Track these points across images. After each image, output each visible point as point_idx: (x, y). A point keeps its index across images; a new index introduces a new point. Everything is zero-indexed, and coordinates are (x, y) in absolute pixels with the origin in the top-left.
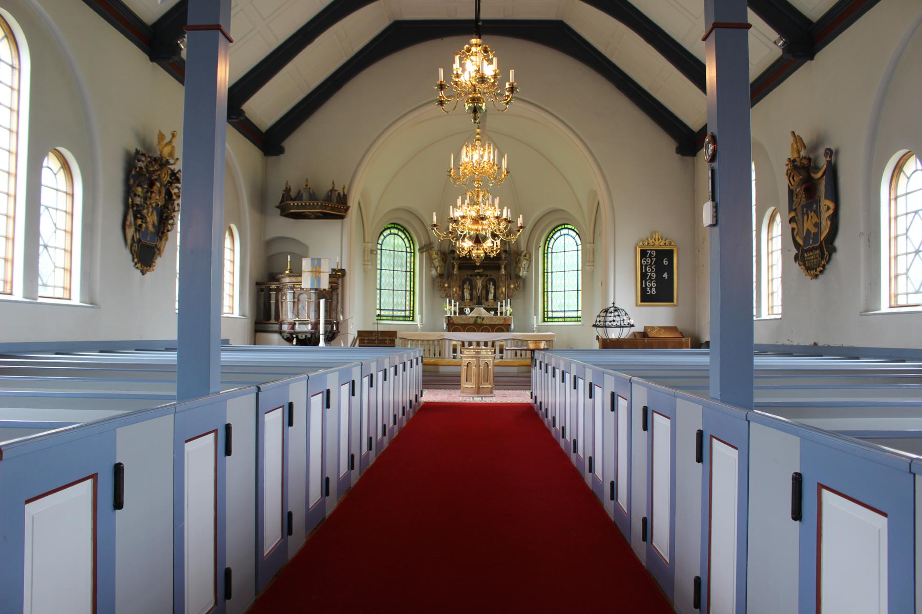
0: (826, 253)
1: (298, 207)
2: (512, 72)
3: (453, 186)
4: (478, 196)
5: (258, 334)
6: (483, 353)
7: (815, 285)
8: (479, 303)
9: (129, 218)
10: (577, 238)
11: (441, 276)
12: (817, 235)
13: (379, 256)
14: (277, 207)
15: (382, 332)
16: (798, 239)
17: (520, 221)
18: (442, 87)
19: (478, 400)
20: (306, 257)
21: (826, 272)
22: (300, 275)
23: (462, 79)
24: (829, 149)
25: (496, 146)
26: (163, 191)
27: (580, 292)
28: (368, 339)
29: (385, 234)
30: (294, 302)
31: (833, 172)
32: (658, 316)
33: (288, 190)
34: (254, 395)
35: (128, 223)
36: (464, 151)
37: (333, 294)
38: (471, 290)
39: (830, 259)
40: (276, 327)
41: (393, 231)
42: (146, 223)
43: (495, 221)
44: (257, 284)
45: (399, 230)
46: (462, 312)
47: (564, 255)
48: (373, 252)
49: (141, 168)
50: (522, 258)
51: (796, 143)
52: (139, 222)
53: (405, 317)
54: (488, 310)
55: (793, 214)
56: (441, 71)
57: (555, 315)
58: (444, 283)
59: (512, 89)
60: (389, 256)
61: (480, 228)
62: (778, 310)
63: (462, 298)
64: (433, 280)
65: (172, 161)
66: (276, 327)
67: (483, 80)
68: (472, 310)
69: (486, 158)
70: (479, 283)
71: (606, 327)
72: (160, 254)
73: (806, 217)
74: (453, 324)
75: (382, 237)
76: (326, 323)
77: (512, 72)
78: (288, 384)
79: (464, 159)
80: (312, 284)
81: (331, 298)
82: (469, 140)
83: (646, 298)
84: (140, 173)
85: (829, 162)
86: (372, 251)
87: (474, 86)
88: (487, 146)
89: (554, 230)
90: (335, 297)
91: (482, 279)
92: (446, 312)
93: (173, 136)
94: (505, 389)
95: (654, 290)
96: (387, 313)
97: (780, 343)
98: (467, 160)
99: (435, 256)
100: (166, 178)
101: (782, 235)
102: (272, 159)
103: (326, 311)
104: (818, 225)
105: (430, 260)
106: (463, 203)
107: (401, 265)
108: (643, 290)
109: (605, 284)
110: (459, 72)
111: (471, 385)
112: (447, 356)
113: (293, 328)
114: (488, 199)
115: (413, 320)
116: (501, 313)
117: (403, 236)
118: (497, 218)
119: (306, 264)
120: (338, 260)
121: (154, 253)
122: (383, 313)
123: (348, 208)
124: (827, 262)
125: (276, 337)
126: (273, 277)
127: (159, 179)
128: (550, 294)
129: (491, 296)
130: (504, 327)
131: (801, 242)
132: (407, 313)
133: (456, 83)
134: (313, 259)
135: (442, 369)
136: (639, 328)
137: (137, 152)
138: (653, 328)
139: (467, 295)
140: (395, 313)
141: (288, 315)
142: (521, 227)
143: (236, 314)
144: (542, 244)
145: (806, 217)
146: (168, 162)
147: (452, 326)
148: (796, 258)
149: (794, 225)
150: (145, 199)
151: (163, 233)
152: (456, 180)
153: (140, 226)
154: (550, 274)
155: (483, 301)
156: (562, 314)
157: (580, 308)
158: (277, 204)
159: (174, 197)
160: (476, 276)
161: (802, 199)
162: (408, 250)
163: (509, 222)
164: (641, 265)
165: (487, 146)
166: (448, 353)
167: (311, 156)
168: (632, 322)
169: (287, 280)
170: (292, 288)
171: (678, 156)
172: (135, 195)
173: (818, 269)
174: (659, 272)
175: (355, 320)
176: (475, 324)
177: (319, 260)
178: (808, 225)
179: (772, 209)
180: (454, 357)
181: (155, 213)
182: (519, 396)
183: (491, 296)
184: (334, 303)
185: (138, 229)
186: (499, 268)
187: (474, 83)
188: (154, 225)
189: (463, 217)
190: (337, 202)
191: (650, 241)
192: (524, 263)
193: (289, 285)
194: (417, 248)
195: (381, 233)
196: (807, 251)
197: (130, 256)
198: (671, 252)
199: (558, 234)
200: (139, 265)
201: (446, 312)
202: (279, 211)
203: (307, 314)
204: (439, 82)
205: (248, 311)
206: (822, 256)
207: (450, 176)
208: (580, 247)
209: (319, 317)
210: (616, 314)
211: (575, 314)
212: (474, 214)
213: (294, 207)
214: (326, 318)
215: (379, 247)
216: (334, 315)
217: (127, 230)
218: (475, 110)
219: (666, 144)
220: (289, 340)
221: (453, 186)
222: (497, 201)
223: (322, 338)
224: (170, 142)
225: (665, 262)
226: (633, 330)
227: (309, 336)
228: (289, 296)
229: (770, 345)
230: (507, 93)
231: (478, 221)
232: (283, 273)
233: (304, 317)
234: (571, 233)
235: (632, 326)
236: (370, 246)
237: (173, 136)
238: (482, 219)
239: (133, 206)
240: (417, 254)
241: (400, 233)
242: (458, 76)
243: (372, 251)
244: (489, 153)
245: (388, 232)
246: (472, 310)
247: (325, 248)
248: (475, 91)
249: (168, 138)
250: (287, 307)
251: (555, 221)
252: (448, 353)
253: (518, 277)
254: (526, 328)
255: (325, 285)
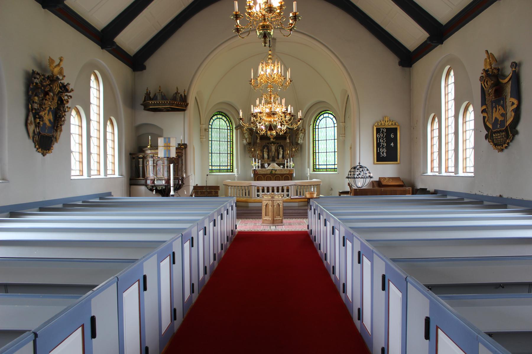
0: (511, 135)
1: (154, 104)
2: (295, 3)
3: (256, 91)
4: (270, 98)
5: (132, 187)
6: (276, 197)
7: (501, 156)
8: (273, 161)
9: (30, 118)
10: (334, 119)
11: (249, 144)
12: (503, 122)
13: (210, 133)
14: (142, 105)
15: (209, 187)
16: (488, 124)
17: (300, 115)
18: (237, 16)
19: (273, 229)
20: (161, 136)
21: (510, 147)
22: (157, 149)
23: (254, 10)
24: (514, 62)
25: (283, 63)
26: (56, 99)
27: (336, 153)
28: (202, 191)
29: (214, 118)
30: (154, 166)
31: (516, 78)
32: (387, 171)
33: (148, 94)
34: (31, 343)
35: (29, 122)
36: (260, 67)
37: (179, 160)
38: (268, 152)
39: (513, 139)
40: (143, 182)
41: (219, 116)
42: (43, 121)
43: (283, 115)
44: (130, 154)
45: (223, 115)
46: (263, 166)
47: (326, 129)
48: (206, 130)
49: (36, 83)
50: (300, 132)
51: (489, 58)
52: (38, 120)
53: (227, 170)
54: (279, 165)
55: (484, 107)
56: (236, 3)
57: (320, 167)
58: (252, 148)
59: (295, 18)
60: (216, 132)
61: (272, 120)
62: (471, 169)
63: (263, 157)
64: (245, 147)
65: (61, 78)
66: (143, 182)
67: (270, 9)
68: (269, 165)
69: (275, 72)
70: (273, 148)
71: (354, 178)
72: (56, 141)
73: (494, 109)
74: (257, 174)
75: (212, 121)
76: (174, 179)
77: (295, 3)
78: (89, 301)
79: (261, 72)
80: (165, 154)
81: (178, 163)
82: (265, 60)
83: (380, 159)
84: (37, 86)
85: (514, 72)
86: (205, 130)
87: (264, 16)
88: (276, 63)
89: (319, 114)
90: (180, 162)
91: (275, 147)
92: (253, 167)
93: (61, 60)
94: (290, 218)
95: (385, 154)
96: (216, 168)
97: (474, 193)
98: (262, 73)
99: (245, 132)
100: (57, 90)
101: (475, 120)
102: (138, 73)
103: (174, 171)
104: (504, 115)
105: (242, 134)
106: (260, 103)
107: (224, 138)
108: (378, 154)
109: (352, 149)
110: (251, 4)
111: (269, 218)
112: (253, 196)
113: (153, 183)
114: (277, 99)
115: (232, 172)
116: (287, 167)
117: (225, 120)
118: (284, 113)
119: (161, 141)
120: (182, 138)
121: (52, 141)
122: (213, 168)
123: (187, 105)
124: (511, 141)
125: (143, 188)
126: (141, 149)
127: (51, 90)
128: (317, 154)
129: (281, 156)
130: (288, 177)
131: (491, 127)
132: (229, 167)
133: (249, 14)
134: (165, 138)
135: (250, 205)
136: (376, 179)
137: (34, 72)
138: (385, 178)
139: (266, 156)
140: (221, 168)
141: (151, 174)
142: (301, 119)
143: (117, 175)
144: (312, 123)
145: (494, 109)
146: (58, 79)
147: (258, 177)
148: (486, 137)
149: (485, 115)
150: (41, 105)
151: (57, 127)
152: (255, 87)
153: (39, 123)
154: (317, 142)
155: (276, 159)
156: (325, 167)
157: (336, 163)
158: (142, 103)
159: (65, 102)
160: (271, 143)
161: (490, 98)
162: (229, 128)
163: (293, 116)
164: (377, 138)
165: (276, 63)
166: (254, 192)
167: (162, 71)
168: (371, 175)
169: (149, 152)
170: (152, 157)
171: (400, 68)
172: (33, 102)
173: (504, 146)
174: (388, 143)
175: (195, 178)
176: (271, 173)
177: (169, 138)
178: (496, 115)
179: (466, 103)
180: (258, 196)
181: (51, 113)
182: (299, 224)
183: (281, 156)
184: (180, 166)
185: (37, 125)
186: (286, 139)
187: (264, 13)
188: (50, 120)
189: (261, 113)
190: (180, 101)
191: (382, 123)
192: (301, 135)
193: (151, 155)
194: (234, 126)
195: (212, 118)
196: (495, 133)
197: (33, 144)
198: (396, 129)
199: (322, 117)
200: (40, 150)
201: (253, 167)
202: (143, 107)
203: (162, 173)
204: (234, 13)
205: (124, 173)
206: (507, 136)
207: (251, 84)
208: (336, 125)
209: (170, 176)
210: (361, 169)
211: (333, 167)
212: (268, 110)
213: (151, 105)
214: (174, 175)
215: (210, 126)
216: (180, 173)
217: (29, 127)
218: (265, 36)
219: (392, 60)
220: (151, 190)
221: (256, 91)
222: (283, 101)
223: (172, 189)
224: (59, 65)
225: (392, 136)
226: (372, 180)
227: (164, 188)
228: (150, 162)
229: (466, 194)
230: (291, 22)
231: (271, 112)
232: (147, 147)
233: (160, 175)
234: (330, 116)
235: (371, 177)
236: (204, 126)
237: (61, 60)
238: (274, 114)
239: (32, 110)
240: (234, 131)
241: (223, 118)
242: (250, 8)
243: (205, 130)
244: (278, 68)
245: (216, 117)
246: (269, 165)
247: (174, 130)
248: (265, 20)
249: (57, 62)
250: (149, 169)
251: (319, 109)
252: (254, 192)
253: (297, 144)
254: (303, 177)
255: (173, 155)
